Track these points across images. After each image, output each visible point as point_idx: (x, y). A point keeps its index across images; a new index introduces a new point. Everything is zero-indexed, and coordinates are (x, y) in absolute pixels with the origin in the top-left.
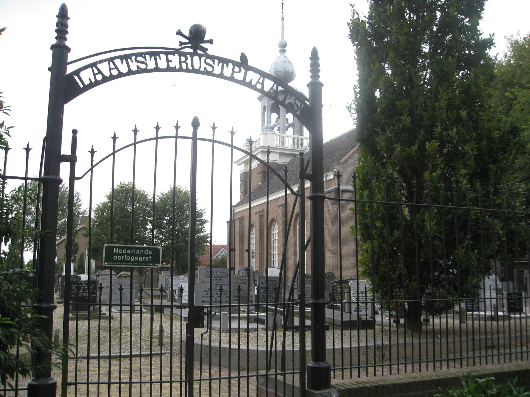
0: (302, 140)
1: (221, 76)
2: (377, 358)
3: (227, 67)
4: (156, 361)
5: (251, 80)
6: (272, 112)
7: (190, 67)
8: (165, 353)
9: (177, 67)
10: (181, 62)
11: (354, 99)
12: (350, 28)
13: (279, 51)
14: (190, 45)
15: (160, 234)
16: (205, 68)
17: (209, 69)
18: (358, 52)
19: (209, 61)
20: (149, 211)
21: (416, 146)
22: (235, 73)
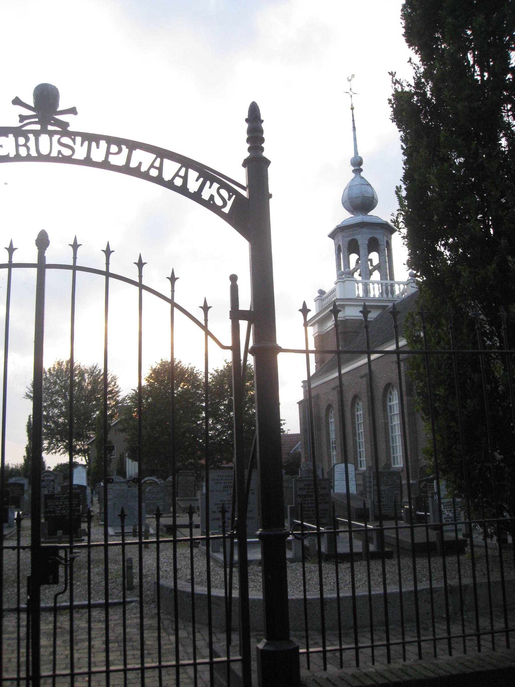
0: (392, 286)
1: (88, 162)
2: (451, 608)
3: (98, 147)
4: (115, 616)
5: (140, 164)
6: (350, 252)
7: (33, 153)
8: (131, 602)
9: (12, 155)
10: (17, 146)
11: (398, 207)
12: (392, 107)
13: (353, 171)
14: (37, 120)
15: (216, 423)
16: (59, 152)
17: (67, 152)
18: (404, 140)
19: (66, 140)
20: (201, 395)
21: (494, 266)
22: (110, 156)
